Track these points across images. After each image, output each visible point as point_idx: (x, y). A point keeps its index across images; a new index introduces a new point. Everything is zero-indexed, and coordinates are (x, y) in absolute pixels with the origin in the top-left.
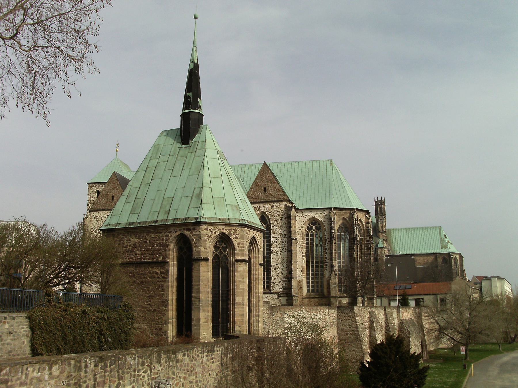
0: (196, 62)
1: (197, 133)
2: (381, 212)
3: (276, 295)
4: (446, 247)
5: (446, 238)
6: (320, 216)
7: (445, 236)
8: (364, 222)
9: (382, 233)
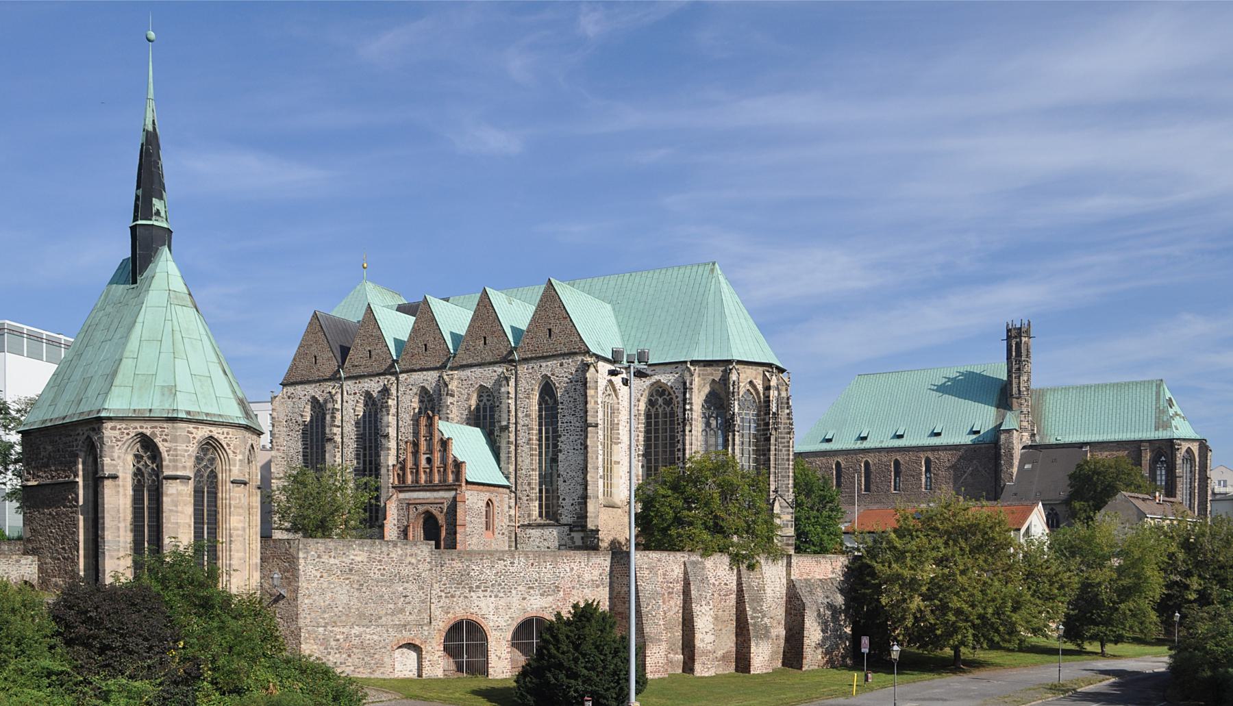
0: (150, 128)
1: (151, 262)
2: (1019, 354)
3: (567, 528)
4: (1167, 425)
6: (668, 379)
8: (760, 388)
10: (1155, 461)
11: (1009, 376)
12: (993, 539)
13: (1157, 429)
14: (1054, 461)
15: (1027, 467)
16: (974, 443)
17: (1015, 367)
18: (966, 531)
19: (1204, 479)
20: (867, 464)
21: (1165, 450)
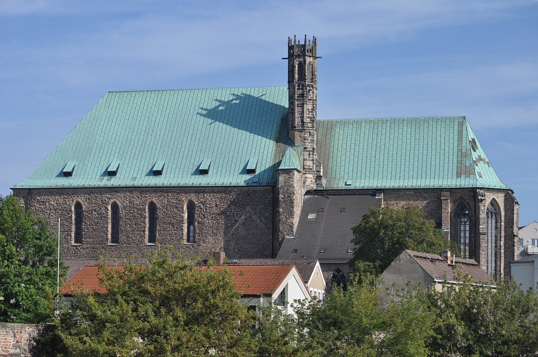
2: (302, 76)
9: (301, 131)
10: (457, 214)
11: (291, 103)
12: (216, 307)
13: (459, 175)
14: (343, 210)
15: (311, 216)
16: (249, 185)
17: (298, 92)
18: (183, 297)
19: (510, 237)
20: (115, 207)
21: (467, 201)
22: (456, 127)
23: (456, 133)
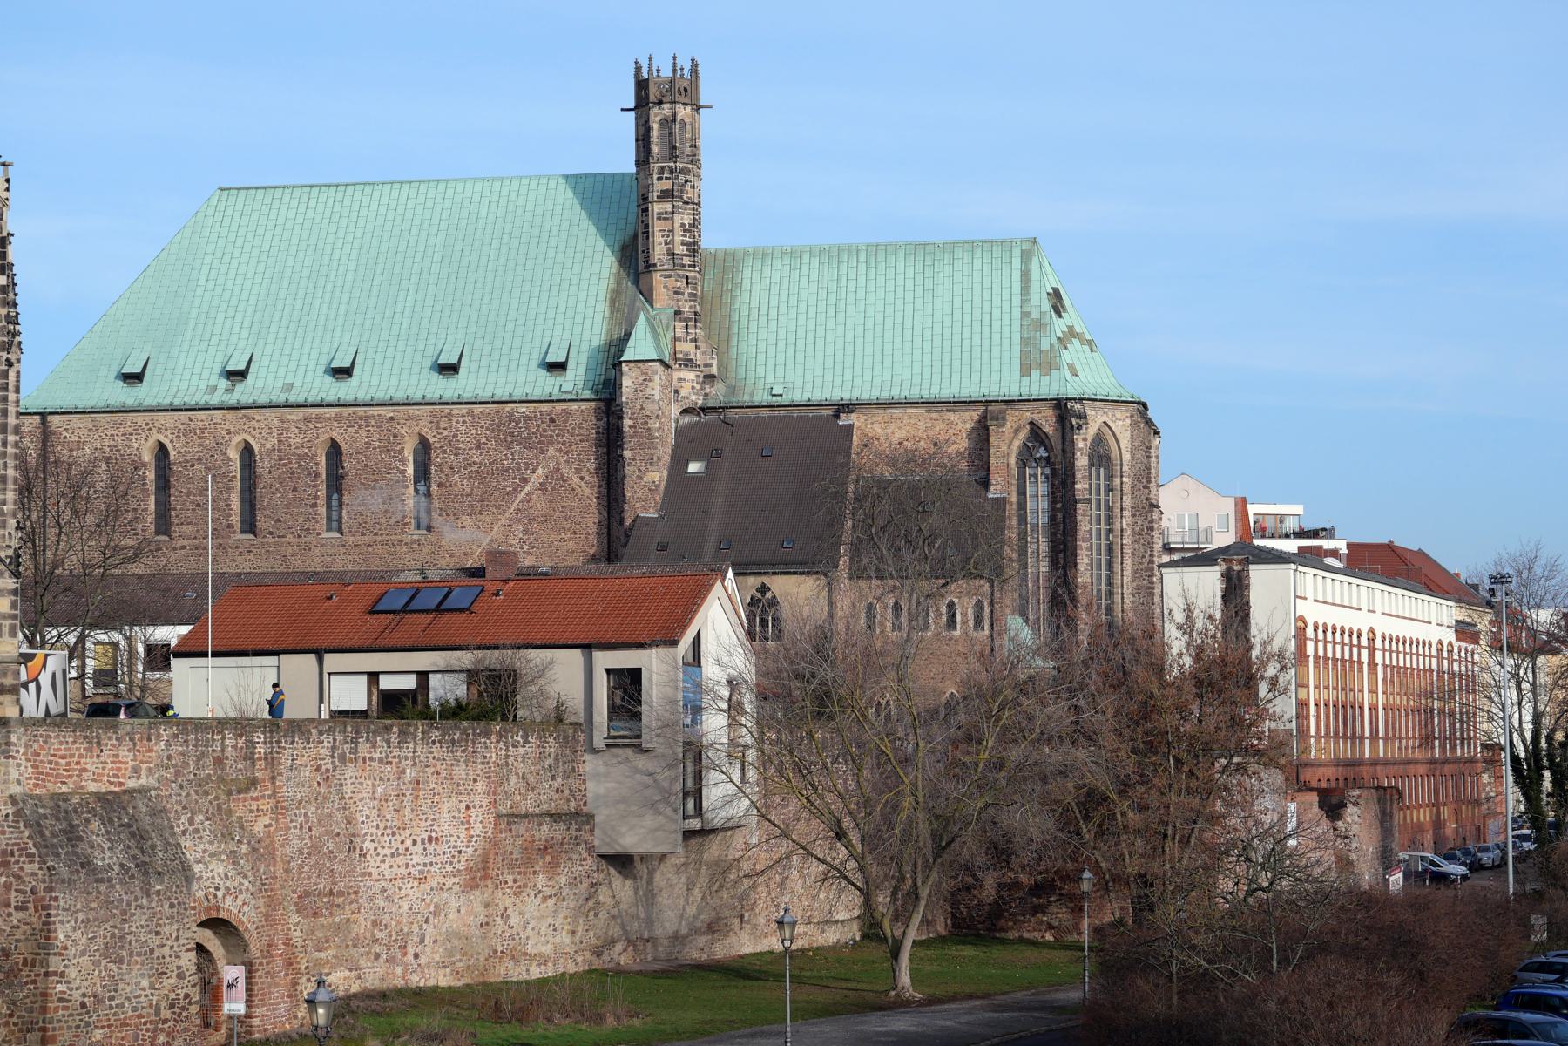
5: (1058, 309)
7: (1056, 294)
15: (694, 467)
20: (247, 451)
22: (1017, 263)
23: (1017, 276)
